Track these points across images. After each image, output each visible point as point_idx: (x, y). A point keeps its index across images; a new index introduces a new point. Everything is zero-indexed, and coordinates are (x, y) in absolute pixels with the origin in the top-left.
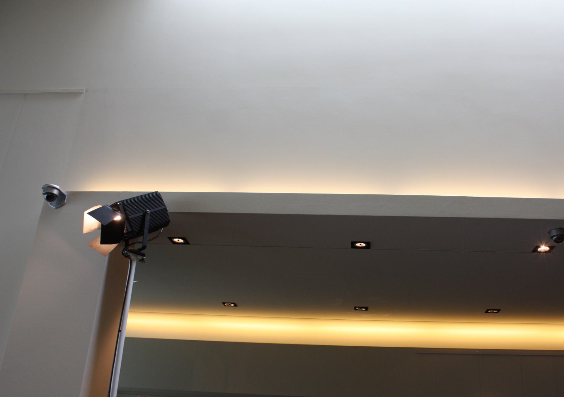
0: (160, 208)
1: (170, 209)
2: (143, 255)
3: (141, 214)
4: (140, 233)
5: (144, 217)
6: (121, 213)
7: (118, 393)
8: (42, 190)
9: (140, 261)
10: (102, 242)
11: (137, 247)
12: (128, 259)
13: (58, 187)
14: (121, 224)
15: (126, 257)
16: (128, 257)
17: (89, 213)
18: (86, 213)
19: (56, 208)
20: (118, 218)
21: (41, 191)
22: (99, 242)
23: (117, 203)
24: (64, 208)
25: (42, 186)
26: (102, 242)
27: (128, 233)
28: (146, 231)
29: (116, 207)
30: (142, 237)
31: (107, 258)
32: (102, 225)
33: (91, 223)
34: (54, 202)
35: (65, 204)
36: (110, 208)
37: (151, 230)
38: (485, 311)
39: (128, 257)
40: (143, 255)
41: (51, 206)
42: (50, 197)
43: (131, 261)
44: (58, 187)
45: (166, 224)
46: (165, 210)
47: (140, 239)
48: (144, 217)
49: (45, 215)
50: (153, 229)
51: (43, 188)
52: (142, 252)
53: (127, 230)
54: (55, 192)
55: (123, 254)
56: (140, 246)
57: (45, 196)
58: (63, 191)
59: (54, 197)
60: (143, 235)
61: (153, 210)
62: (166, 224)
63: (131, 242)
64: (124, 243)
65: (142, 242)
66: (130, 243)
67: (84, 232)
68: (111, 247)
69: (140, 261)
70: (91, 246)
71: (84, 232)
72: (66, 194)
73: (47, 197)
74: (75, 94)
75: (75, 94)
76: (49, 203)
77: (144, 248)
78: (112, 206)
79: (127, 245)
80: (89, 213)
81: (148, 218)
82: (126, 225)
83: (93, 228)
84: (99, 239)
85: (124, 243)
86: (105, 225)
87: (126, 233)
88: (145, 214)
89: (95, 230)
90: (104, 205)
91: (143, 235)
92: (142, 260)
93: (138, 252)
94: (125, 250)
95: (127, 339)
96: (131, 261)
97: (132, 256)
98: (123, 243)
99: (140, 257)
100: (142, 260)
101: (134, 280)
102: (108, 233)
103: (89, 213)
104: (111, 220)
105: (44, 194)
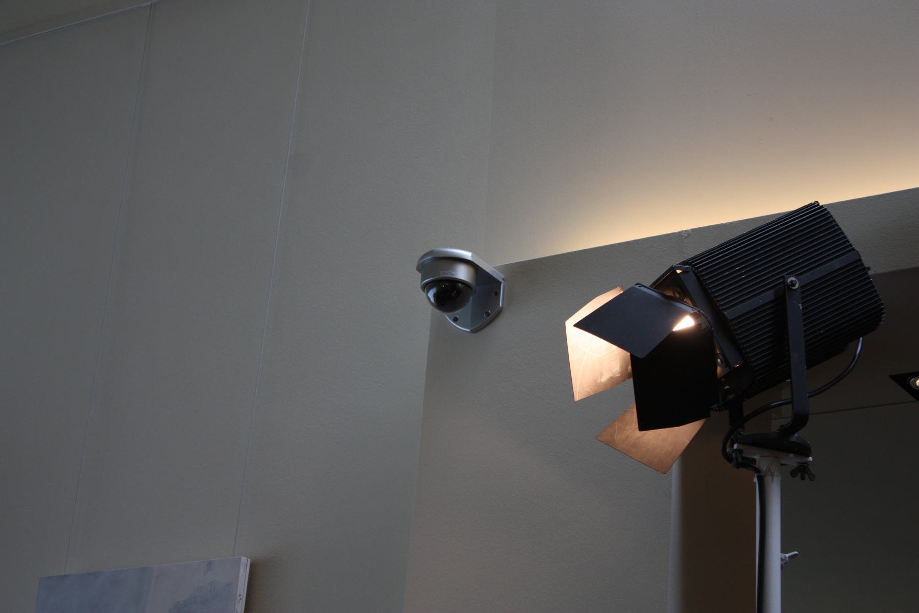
0: (836, 264)
2: (803, 450)
3: (769, 296)
4: (776, 371)
5: (779, 305)
6: (695, 304)
8: (419, 275)
9: (793, 473)
10: (643, 427)
12: (742, 470)
13: (467, 253)
15: (739, 465)
16: (749, 464)
17: (579, 325)
18: (570, 323)
19: (474, 331)
22: (635, 425)
23: (672, 270)
24: (502, 328)
26: (643, 427)
27: (732, 373)
28: (797, 356)
29: (673, 287)
32: (634, 359)
33: (594, 360)
34: (464, 312)
35: (500, 312)
37: (818, 354)
39: (749, 464)
40: (803, 450)
41: (457, 325)
42: (448, 295)
43: (761, 480)
44: (467, 255)
45: (869, 319)
46: (858, 267)
48: (779, 305)
51: (421, 268)
52: (795, 438)
53: (726, 363)
54: (462, 273)
55: (728, 457)
57: (431, 294)
59: (459, 292)
61: (809, 277)
62: (869, 319)
63: (749, 406)
64: (726, 413)
65: (791, 402)
66: (746, 413)
67: (577, 398)
68: (677, 437)
69: (793, 473)
70: (610, 444)
71: (577, 398)
72: (498, 276)
73: (436, 296)
76: (448, 317)
77: (800, 421)
78: (658, 285)
79: (738, 420)
82: (721, 346)
83: (604, 378)
84: (633, 416)
85: (726, 413)
86: (641, 355)
88: (782, 295)
89: (614, 383)
92: (802, 471)
93: (783, 443)
94: (730, 438)
96: (761, 480)
97: (762, 459)
99: (792, 461)
100: (802, 471)
101: (784, 550)
102: (661, 383)
103: (579, 325)
104: (664, 336)
105: (426, 287)
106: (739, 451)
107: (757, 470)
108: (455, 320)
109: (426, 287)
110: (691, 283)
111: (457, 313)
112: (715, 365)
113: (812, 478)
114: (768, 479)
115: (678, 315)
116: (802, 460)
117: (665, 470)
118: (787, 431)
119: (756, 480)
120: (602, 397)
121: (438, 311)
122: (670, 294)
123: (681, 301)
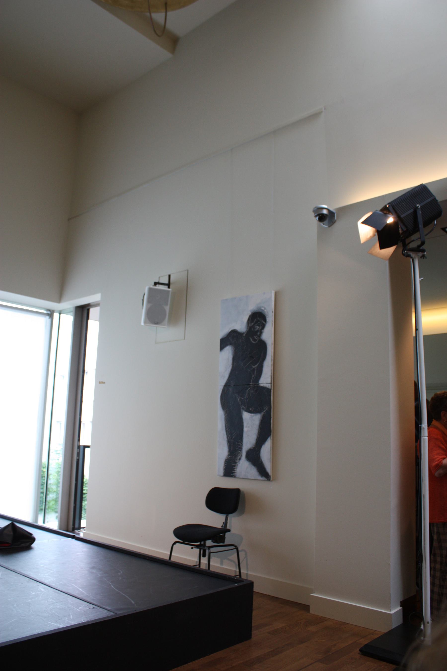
0: (429, 200)
1: (440, 198)
2: (423, 251)
3: (412, 210)
4: (416, 229)
6: (392, 214)
7: (427, 390)
9: (421, 257)
10: (382, 247)
11: (413, 245)
12: (408, 258)
14: (395, 224)
16: (409, 256)
18: (359, 223)
20: (390, 220)
21: (313, 215)
23: (386, 206)
24: (337, 226)
25: (312, 210)
26: (382, 247)
27: (404, 232)
28: (421, 226)
29: (386, 210)
30: (418, 233)
31: (387, 262)
32: (378, 231)
33: (366, 232)
34: (326, 222)
35: (335, 221)
36: (381, 213)
38: (101, 381)
39: (409, 256)
40: (423, 251)
41: (324, 226)
42: (322, 218)
44: (325, 206)
46: (435, 200)
47: (414, 237)
49: (321, 235)
50: (427, 223)
51: (314, 211)
52: (421, 248)
53: (402, 229)
54: (325, 212)
55: (404, 255)
56: (419, 243)
57: (317, 218)
58: (331, 209)
60: (418, 230)
61: (422, 204)
65: (420, 238)
68: (390, 251)
69: (421, 257)
70: (371, 254)
72: (334, 211)
74: (316, 115)
75: (316, 115)
76: (321, 224)
77: (423, 243)
78: (382, 210)
79: (405, 246)
80: (364, 222)
81: (420, 213)
82: (400, 225)
83: (369, 236)
84: (378, 245)
86: (380, 229)
87: (402, 233)
88: (416, 209)
90: (374, 211)
91: (418, 230)
92: (423, 256)
93: (418, 249)
94: (403, 250)
95: (425, 337)
98: (400, 244)
99: (420, 254)
100: (423, 256)
101: (420, 278)
102: (385, 237)
103: (364, 222)
104: (383, 226)
105: (316, 216)
106: (407, 253)
107: (412, 257)
108: (324, 224)
109: (316, 216)
110: (391, 209)
111: (324, 222)
112: (399, 230)
113: (426, 258)
114: (415, 260)
115: (387, 218)
116: (423, 253)
117: (49, 507)
118: (419, 246)
119: (411, 260)
120: (369, 241)
121: (319, 223)
122: (385, 212)
123: (388, 214)
